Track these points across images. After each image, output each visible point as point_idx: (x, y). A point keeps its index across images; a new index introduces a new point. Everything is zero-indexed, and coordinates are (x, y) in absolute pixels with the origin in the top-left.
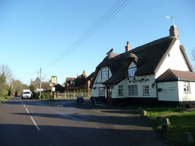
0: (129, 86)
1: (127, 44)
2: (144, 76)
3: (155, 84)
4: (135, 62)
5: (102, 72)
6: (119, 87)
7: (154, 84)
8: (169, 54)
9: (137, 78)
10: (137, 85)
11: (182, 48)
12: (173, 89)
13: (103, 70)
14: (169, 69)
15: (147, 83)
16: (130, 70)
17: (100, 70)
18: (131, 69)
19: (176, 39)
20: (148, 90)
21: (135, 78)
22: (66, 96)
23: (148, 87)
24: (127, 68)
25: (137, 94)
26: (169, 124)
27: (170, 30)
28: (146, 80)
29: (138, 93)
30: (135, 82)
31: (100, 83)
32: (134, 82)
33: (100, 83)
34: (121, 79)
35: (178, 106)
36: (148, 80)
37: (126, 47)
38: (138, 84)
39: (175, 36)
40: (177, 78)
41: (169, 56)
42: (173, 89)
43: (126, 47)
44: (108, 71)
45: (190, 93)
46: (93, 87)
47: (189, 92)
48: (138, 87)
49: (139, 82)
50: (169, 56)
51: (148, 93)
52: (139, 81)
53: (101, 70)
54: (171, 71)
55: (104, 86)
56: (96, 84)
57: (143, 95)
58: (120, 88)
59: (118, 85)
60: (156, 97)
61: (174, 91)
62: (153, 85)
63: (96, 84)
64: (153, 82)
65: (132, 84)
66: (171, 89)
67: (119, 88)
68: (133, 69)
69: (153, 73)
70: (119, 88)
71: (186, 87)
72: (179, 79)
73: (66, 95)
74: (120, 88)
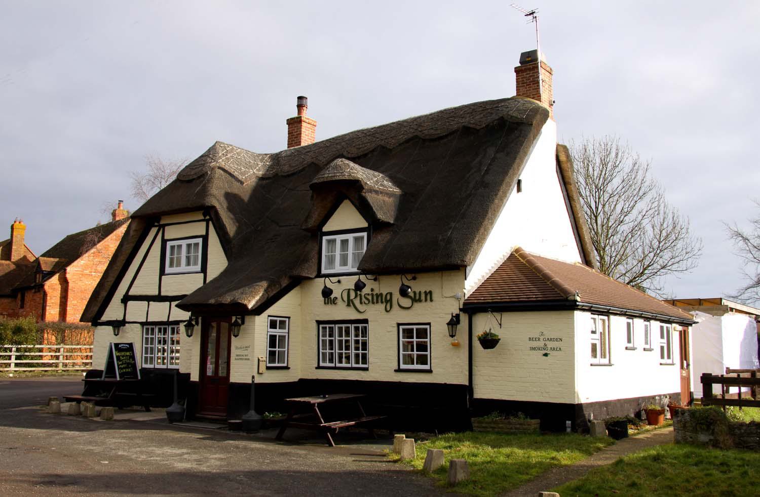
0: (319, 323)
1: (300, 106)
2: (410, 276)
3: (464, 319)
4: (365, 209)
5: (164, 242)
6: (273, 325)
7: (458, 316)
8: (519, 182)
9: (370, 285)
10: (366, 321)
11: (563, 158)
12: (550, 345)
13: (170, 232)
14: (517, 251)
15: (418, 314)
16: (329, 241)
17: (154, 231)
18: (339, 238)
19: (545, 115)
20: (422, 347)
21: (359, 286)
22: (17, 365)
23: (422, 333)
24: (316, 234)
25: (364, 362)
26: (221, 459)
27: (517, 70)
28: (416, 299)
29: (371, 358)
30: (357, 302)
31: (148, 299)
32: (350, 303)
33: (148, 299)
34: (285, 283)
35: (569, 423)
36: (429, 295)
37: (295, 124)
38: (374, 313)
39: (538, 97)
40: (571, 298)
41: (519, 190)
42: (550, 345)
43: (295, 124)
44: (205, 238)
45: (610, 365)
46: (105, 318)
47: (606, 361)
48: (371, 327)
49: (381, 307)
50: (519, 190)
51: (423, 360)
52: (377, 298)
53: (162, 227)
54: (529, 262)
55: (186, 315)
56: (126, 299)
57: (399, 370)
58: (277, 332)
59: (265, 315)
60: (467, 383)
61: (554, 353)
62: (454, 322)
63: (126, 299)
64: (454, 308)
65: (341, 312)
66: (541, 344)
67: (273, 332)
68: (350, 237)
69: (460, 268)
70: (273, 332)
71: (597, 336)
72: (578, 299)
73: (13, 360)
74: (277, 332)
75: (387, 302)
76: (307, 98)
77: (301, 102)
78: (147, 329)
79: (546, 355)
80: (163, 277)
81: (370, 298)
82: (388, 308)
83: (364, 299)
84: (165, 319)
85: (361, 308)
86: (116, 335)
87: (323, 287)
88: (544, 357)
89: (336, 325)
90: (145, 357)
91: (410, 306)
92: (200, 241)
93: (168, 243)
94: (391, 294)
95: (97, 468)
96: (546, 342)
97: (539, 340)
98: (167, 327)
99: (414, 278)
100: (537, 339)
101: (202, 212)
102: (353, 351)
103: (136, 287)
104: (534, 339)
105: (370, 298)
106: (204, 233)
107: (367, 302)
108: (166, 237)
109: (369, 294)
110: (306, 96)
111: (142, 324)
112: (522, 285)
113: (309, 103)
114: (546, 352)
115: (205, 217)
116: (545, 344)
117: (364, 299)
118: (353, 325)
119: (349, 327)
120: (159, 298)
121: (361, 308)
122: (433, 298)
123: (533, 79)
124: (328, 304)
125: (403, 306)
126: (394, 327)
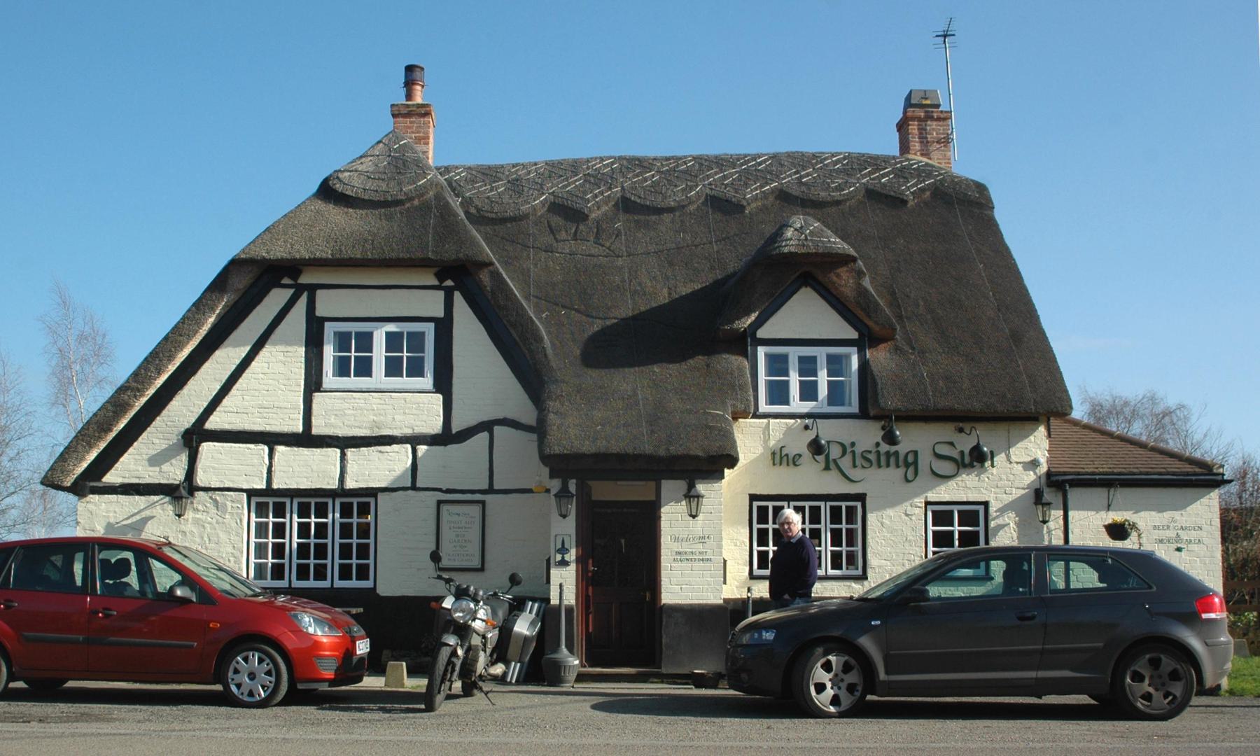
1: (409, 84)
10: (861, 498)
44: (444, 328)
49: (895, 474)
63: (195, 437)
66: (1171, 534)
75: (907, 465)
76: (422, 69)
77: (411, 74)
78: (259, 505)
79: (1179, 549)
80: (317, 397)
81: (872, 457)
82: (910, 477)
83: (859, 461)
84: (334, 485)
85: (854, 474)
86: (694, 517)
87: (814, 437)
88: (1177, 552)
89: (791, 503)
90: (759, 552)
91: (954, 474)
92: (429, 329)
93: (327, 324)
94: (916, 453)
95: (1130, 724)
96: (1179, 531)
97: (1168, 527)
98: (330, 502)
99: (961, 430)
100: (1165, 528)
101: (436, 270)
102: (829, 548)
103: (219, 412)
104: (1161, 527)
105: (872, 457)
106: (440, 313)
107: (866, 464)
108: (320, 312)
109: (870, 452)
110: (422, 65)
111: (251, 493)
112: (1054, 449)
113: (428, 76)
114: (1179, 545)
115: (441, 281)
116: (1177, 534)
117: (859, 461)
118: (829, 504)
119: (819, 508)
120: (306, 439)
121: (854, 474)
122: (995, 463)
123: (944, 130)
124: (888, 465)
125: (939, 473)
126: (919, 507)
